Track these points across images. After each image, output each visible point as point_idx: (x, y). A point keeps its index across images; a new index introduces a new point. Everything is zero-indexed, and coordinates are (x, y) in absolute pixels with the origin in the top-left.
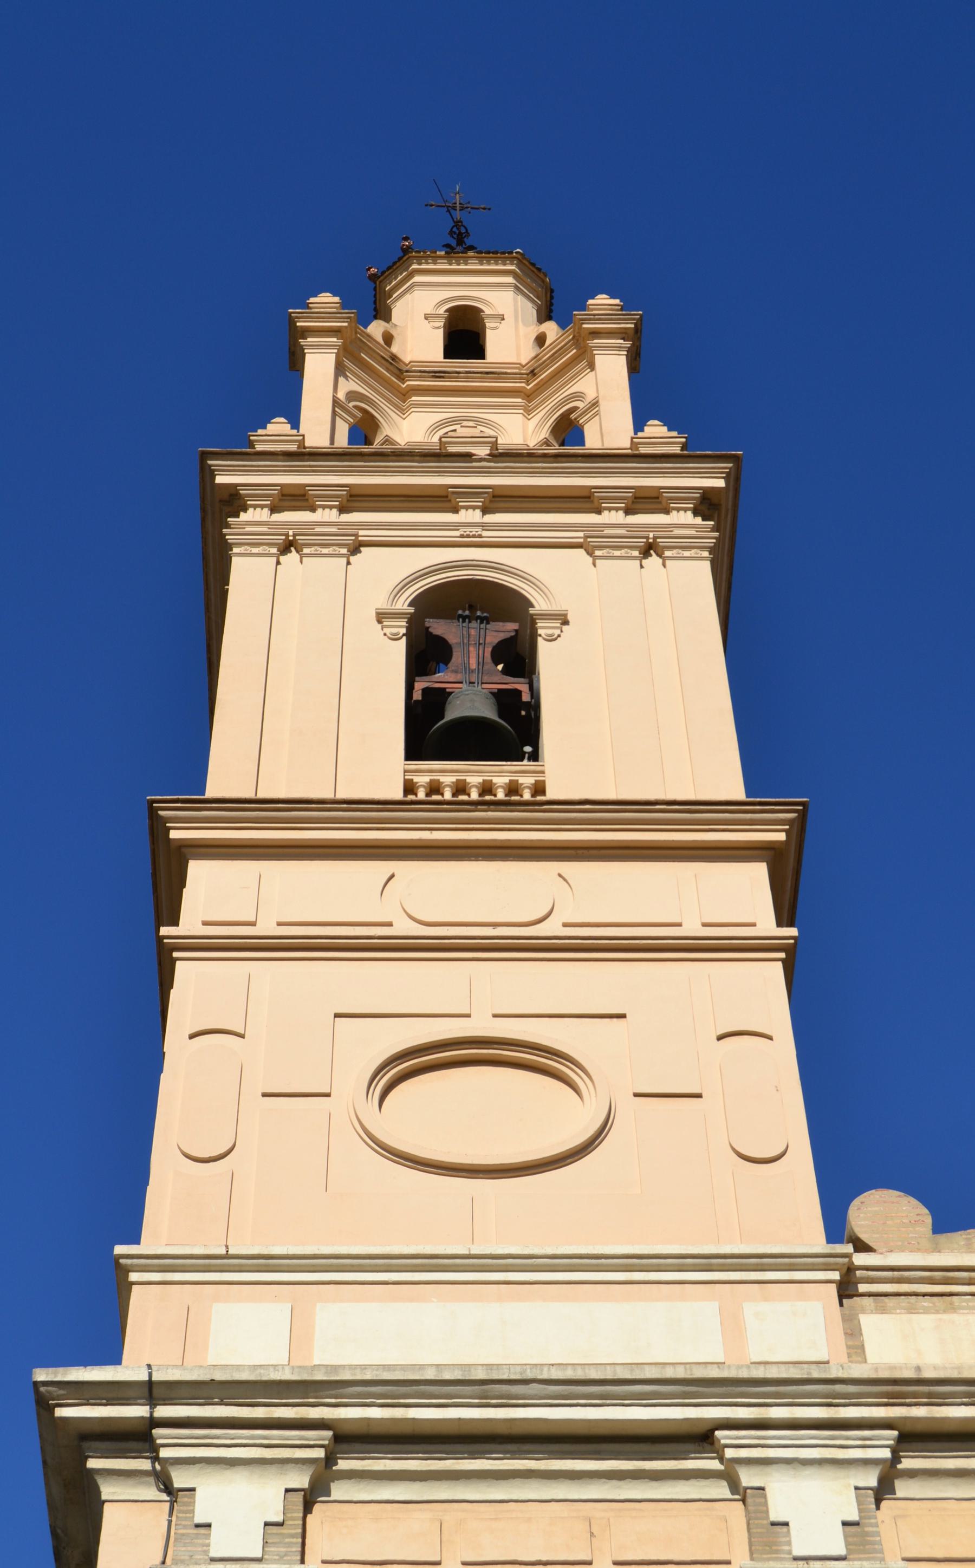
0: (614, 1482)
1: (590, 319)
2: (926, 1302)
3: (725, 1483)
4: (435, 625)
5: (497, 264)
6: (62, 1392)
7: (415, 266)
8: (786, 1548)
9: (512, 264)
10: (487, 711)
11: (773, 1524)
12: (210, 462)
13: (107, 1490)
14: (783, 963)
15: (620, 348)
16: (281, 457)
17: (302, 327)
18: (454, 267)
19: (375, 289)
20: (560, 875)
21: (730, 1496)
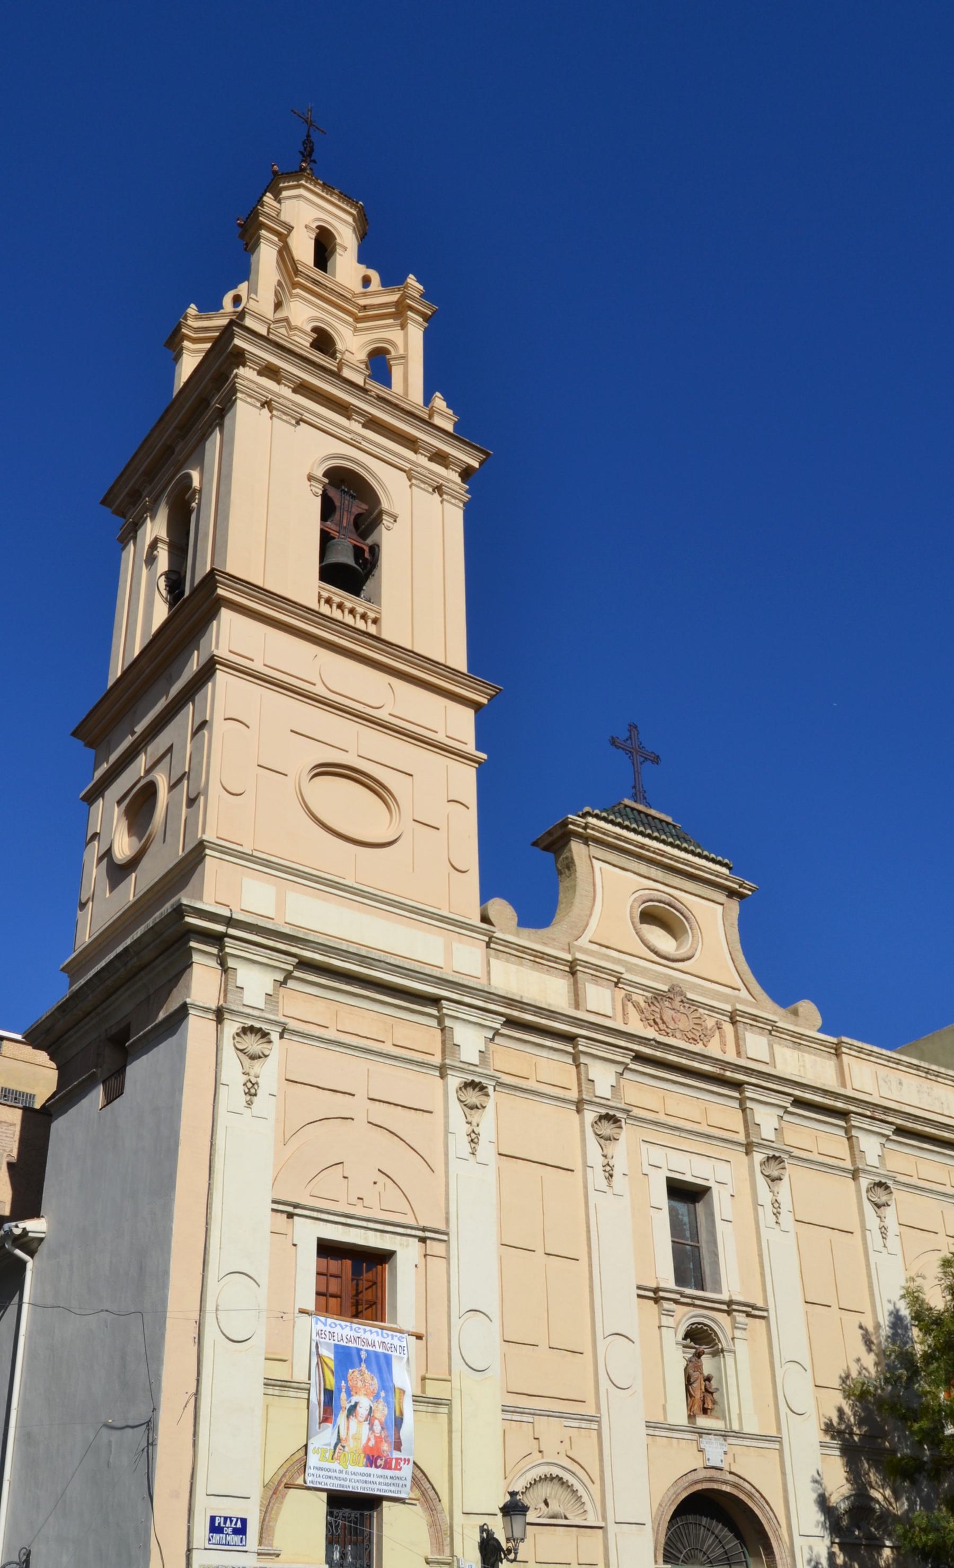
0: (397, 1009)
1: (411, 298)
2: (513, 959)
3: (436, 1021)
4: (330, 490)
5: (347, 205)
6: (191, 911)
7: (303, 182)
8: (458, 1056)
9: (355, 210)
10: (351, 561)
11: (455, 1045)
12: (235, 328)
13: (196, 958)
14: (479, 771)
15: (421, 325)
16: (272, 344)
17: (261, 221)
18: (324, 194)
19: (272, 180)
20: (389, 684)
21: (437, 1026)
